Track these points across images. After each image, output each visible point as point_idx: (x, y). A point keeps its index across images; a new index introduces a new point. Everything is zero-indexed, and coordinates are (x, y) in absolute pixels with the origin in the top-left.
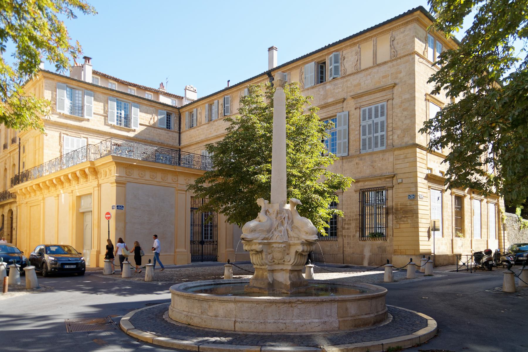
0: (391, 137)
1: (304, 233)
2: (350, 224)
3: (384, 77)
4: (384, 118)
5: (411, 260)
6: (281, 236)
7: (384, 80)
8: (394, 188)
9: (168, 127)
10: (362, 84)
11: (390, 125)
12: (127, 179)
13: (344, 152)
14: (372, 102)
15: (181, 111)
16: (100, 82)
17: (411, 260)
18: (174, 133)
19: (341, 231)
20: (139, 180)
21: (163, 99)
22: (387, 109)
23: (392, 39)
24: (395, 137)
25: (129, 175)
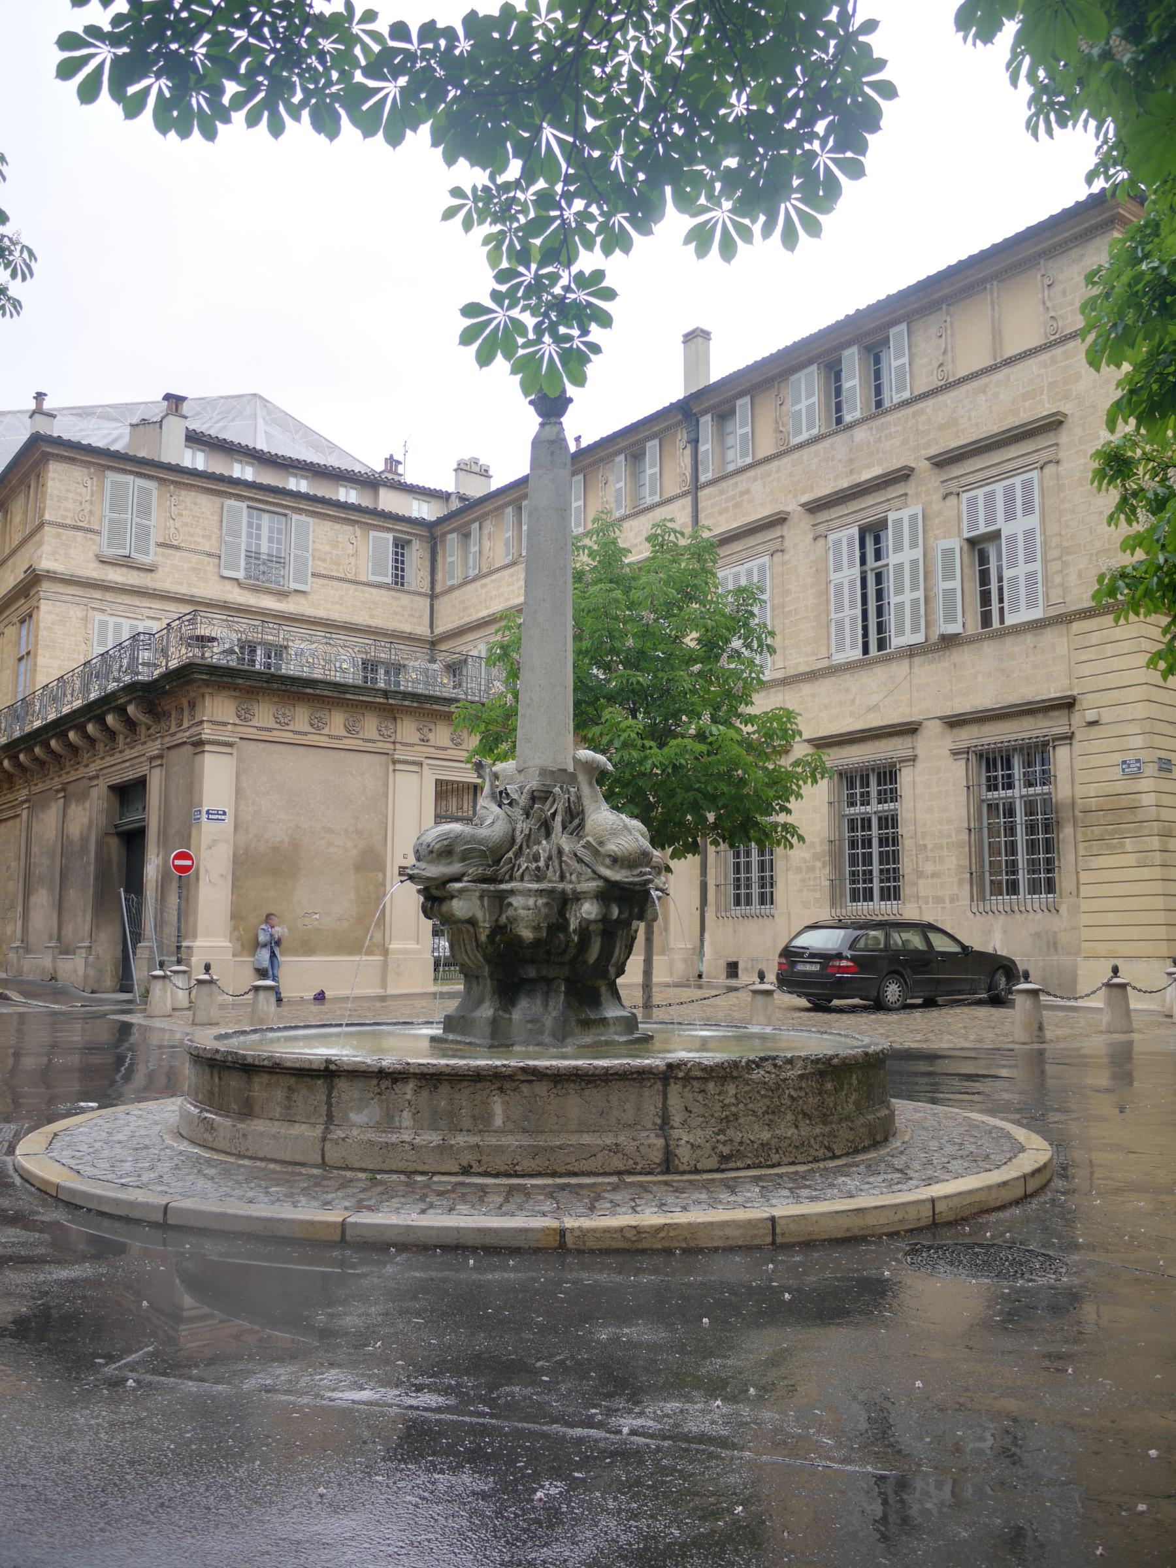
0: (1058, 579)
1: (607, 861)
2: (941, 858)
3: (1025, 396)
4: (1033, 521)
5: (1115, 970)
6: (538, 868)
7: (1027, 404)
8: (1075, 742)
9: (399, 579)
11: (1055, 541)
12: (240, 729)
13: (915, 629)
14: (994, 471)
15: (439, 531)
16: (198, 460)
17: (1115, 970)
18: (418, 598)
19: (915, 884)
20: (275, 733)
21: (388, 501)
22: (1042, 491)
24: (1073, 578)
25: (245, 720)
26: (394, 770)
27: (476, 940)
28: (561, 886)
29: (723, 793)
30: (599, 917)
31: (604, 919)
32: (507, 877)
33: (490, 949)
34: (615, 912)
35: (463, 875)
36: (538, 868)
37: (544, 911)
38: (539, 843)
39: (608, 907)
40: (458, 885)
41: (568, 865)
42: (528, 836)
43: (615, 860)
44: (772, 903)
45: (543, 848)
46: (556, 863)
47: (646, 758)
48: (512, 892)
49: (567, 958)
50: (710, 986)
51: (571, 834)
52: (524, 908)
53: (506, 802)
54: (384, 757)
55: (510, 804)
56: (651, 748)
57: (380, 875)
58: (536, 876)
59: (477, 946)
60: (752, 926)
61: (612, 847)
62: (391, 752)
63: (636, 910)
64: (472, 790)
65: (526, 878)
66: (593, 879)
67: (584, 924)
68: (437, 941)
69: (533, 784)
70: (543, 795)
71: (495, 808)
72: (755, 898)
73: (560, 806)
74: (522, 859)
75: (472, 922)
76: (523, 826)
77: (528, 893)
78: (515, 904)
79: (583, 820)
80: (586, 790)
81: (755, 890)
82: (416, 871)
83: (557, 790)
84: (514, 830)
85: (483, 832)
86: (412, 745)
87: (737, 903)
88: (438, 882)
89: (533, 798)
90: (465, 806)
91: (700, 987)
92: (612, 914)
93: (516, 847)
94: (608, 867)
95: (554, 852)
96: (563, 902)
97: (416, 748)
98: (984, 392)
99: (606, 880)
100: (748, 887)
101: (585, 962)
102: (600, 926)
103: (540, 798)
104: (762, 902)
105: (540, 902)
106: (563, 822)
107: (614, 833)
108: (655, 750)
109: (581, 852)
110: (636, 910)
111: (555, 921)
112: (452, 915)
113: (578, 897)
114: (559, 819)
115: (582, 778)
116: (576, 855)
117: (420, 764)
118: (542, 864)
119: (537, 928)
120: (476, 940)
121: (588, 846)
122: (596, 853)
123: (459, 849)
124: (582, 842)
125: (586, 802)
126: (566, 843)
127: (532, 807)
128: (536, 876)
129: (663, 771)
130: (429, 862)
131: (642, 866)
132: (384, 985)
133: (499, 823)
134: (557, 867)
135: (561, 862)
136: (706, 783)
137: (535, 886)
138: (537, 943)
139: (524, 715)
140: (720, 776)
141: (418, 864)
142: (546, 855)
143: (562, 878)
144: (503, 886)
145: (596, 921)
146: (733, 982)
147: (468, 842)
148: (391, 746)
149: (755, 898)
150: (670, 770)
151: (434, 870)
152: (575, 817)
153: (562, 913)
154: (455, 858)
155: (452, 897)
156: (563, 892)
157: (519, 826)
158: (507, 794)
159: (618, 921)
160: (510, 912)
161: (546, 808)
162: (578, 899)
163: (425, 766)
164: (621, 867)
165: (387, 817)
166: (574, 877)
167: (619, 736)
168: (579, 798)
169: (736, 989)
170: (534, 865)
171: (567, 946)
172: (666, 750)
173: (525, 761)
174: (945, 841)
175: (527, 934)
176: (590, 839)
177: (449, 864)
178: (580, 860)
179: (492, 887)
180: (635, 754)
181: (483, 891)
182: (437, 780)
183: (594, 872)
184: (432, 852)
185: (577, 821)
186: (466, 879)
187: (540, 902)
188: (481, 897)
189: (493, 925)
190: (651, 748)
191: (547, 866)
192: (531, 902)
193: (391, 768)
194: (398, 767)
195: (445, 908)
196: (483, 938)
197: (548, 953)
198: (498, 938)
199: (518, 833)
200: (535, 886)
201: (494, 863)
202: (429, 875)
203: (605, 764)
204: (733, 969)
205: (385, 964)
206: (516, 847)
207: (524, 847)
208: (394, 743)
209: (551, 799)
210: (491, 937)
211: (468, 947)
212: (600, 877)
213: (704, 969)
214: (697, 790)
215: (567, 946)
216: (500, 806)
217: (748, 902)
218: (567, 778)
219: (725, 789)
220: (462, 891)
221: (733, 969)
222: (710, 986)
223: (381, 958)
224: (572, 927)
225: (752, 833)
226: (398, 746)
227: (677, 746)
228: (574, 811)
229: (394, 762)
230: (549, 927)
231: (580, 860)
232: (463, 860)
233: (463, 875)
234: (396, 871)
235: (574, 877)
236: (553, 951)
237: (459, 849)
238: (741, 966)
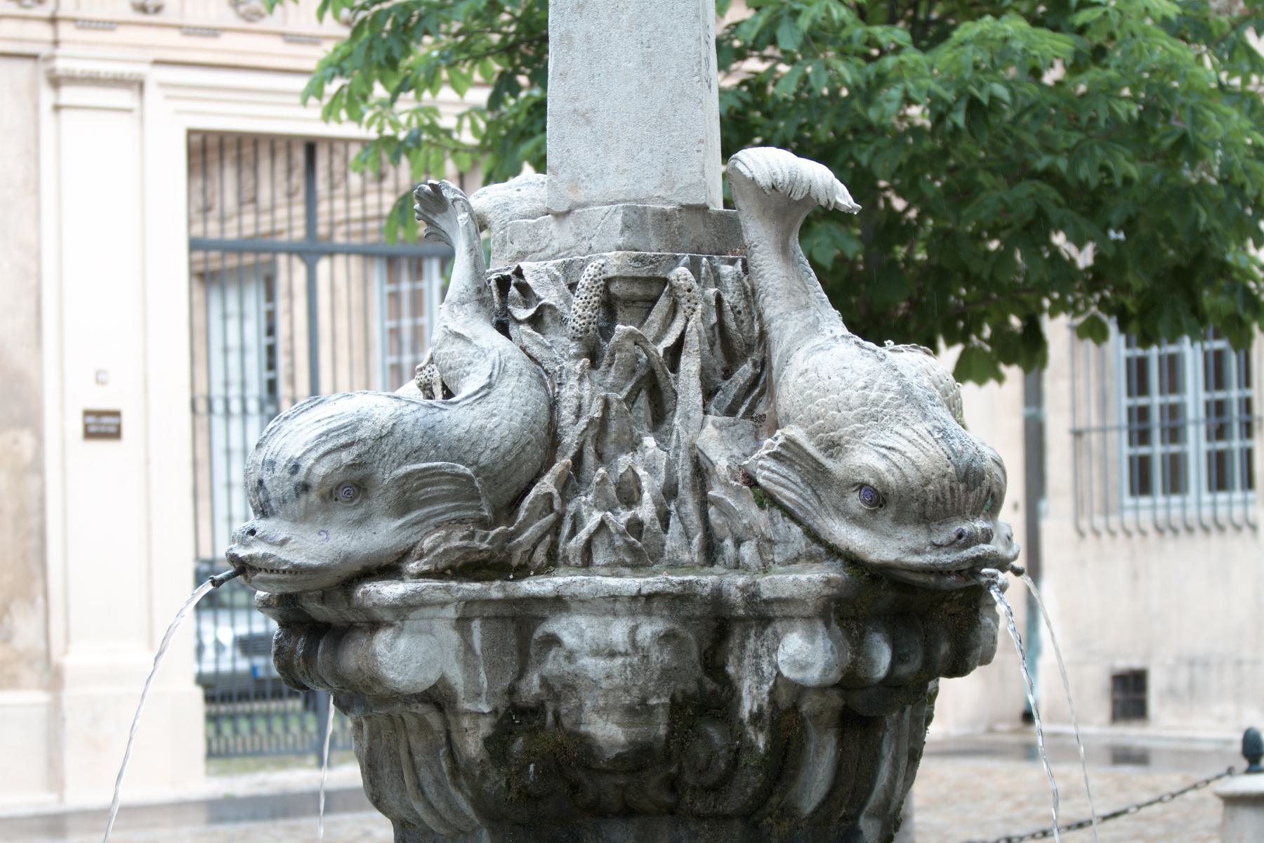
1: (854, 502)
26: (57, 108)
27: (452, 754)
28: (707, 580)
29: (1128, 181)
30: (835, 676)
31: (850, 682)
32: (540, 556)
33: (495, 781)
34: (882, 658)
35: (405, 555)
36: (636, 526)
37: (660, 657)
38: (634, 445)
39: (858, 643)
40: (390, 590)
41: (725, 511)
42: (601, 425)
43: (879, 500)
44: (1249, 483)
45: (649, 460)
46: (690, 507)
47: (882, 80)
48: (559, 603)
49: (734, 801)
50: (1063, 750)
51: (731, 411)
52: (596, 653)
53: (522, 313)
54: (25, 67)
55: (536, 322)
56: (898, 49)
57: (27, 439)
58: (631, 549)
59: (455, 770)
60: (1189, 560)
61: (865, 459)
62: (44, 50)
63: (944, 648)
64: (300, 156)
65: (600, 557)
66: (811, 558)
67: (784, 699)
68: (207, 625)
69: (609, 258)
70: (637, 290)
71: (489, 337)
72: (1197, 471)
73: (694, 324)
74: (584, 501)
75: (438, 698)
76: (582, 394)
77: (610, 604)
78: (569, 639)
79: (764, 364)
80: (771, 270)
81: (1196, 446)
82: (258, 550)
83: (680, 274)
84: (553, 405)
85: (460, 418)
86: (110, 25)
87: (1141, 483)
88: (327, 580)
89: (610, 304)
90: (265, 195)
91: (1029, 752)
92: (872, 664)
93: (562, 463)
94: (856, 520)
95: (683, 472)
96: (717, 629)
97: (123, 34)
99: (852, 561)
100: (1174, 434)
101: (788, 812)
102: (836, 700)
103: (630, 301)
104: (1219, 480)
105: (649, 630)
106: (705, 376)
107: (873, 416)
108: (912, 56)
109: (768, 474)
110: (944, 648)
111: (692, 687)
112: (376, 679)
113: (764, 615)
114: (690, 365)
115: (758, 233)
116: (751, 481)
117: (138, 85)
118: (646, 511)
119: (638, 711)
120: (452, 754)
121: (789, 454)
122: (817, 476)
123: (389, 473)
124: (770, 444)
125: (774, 308)
126: (717, 443)
127: (606, 332)
128: (631, 549)
129: (939, 119)
130: (296, 520)
131: (960, 513)
132: (55, 777)
133: (508, 386)
134: (694, 520)
135: (704, 503)
136: (1074, 153)
137: (630, 583)
138: (638, 758)
139: (567, 38)
140: (1117, 132)
141: (262, 525)
142: (659, 482)
143: (711, 552)
144: (531, 586)
145: (821, 689)
146: (1131, 734)
147: (415, 454)
148: (45, 32)
149: (1197, 471)
150: (959, 118)
151: (313, 545)
152: (741, 363)
153: (713, 664)
154: (378, 502)
155: (375, 625)
156: (718, 598)
157: (569, 394)
158: (524, 289)
159: (892, 683)
160: (553, 665)
161: (650, 332)
162: (764, 621)
163: (150, 88)
164: (899, 520)
165: (38, 256)
166: (748, 551)
167: (795, 14)
168: (750, 295)
169: (1139, 758)
170: (624, 516)
171: (734, 764)
172: (944, 54)
173: (574, 185)
175: (608, 732)
176: (796, 432)
177: (360, 522)
178: (766, 499)
179: (495, 590)
180: (846, 71)
181: (469, 602)
182: (190, 132)
183: (813, 535)
184: (305, 487)
185: (745, 371)
186: (413, 566)
187: (649, 630)
188: (462, 623)
189: (502, 704)
190: (898, 49)
191: (664, 517)
192: (618, 632)
193: (47, 97)
194: (69, 95)
195: (352, 658)
196: (472, 746)
197: (673, 785)
198: (518, 745)
199: (566, 414)
200: (630, 583)
201: (495, 514)
202: (299, 559)
203: (830, 190)
204: (1130, 693)
205: (55, 713)
206: (562, 463)
207: (590, 458)
208: (53, 20)
209: (663, 303)
210: (497, 744)
211: (426, 776)
212: (834, 552)
213: (1044, 695)
214: (1048, 175)
215: (734, 764)
216: (503, 328)
217: (1176, 483)
218: (714, 232)
219: (1134, 171)
220: (404, 608)
221: (1130, 693)
222: (1063, 750)
223: (41, 697)
224: (747, 706)
225: (1208, 298)
226: (66, 30)
227: (982, 39)
228: (738, 338)
229: (56, 82)
230: (676, 707)
231: (766, 499)
232: (403, 507)
233: (405, 555)
234: (76, 426)
235: (748, 551)
236: (689, 778)
237: (389, 473)
238: (1155, 684)
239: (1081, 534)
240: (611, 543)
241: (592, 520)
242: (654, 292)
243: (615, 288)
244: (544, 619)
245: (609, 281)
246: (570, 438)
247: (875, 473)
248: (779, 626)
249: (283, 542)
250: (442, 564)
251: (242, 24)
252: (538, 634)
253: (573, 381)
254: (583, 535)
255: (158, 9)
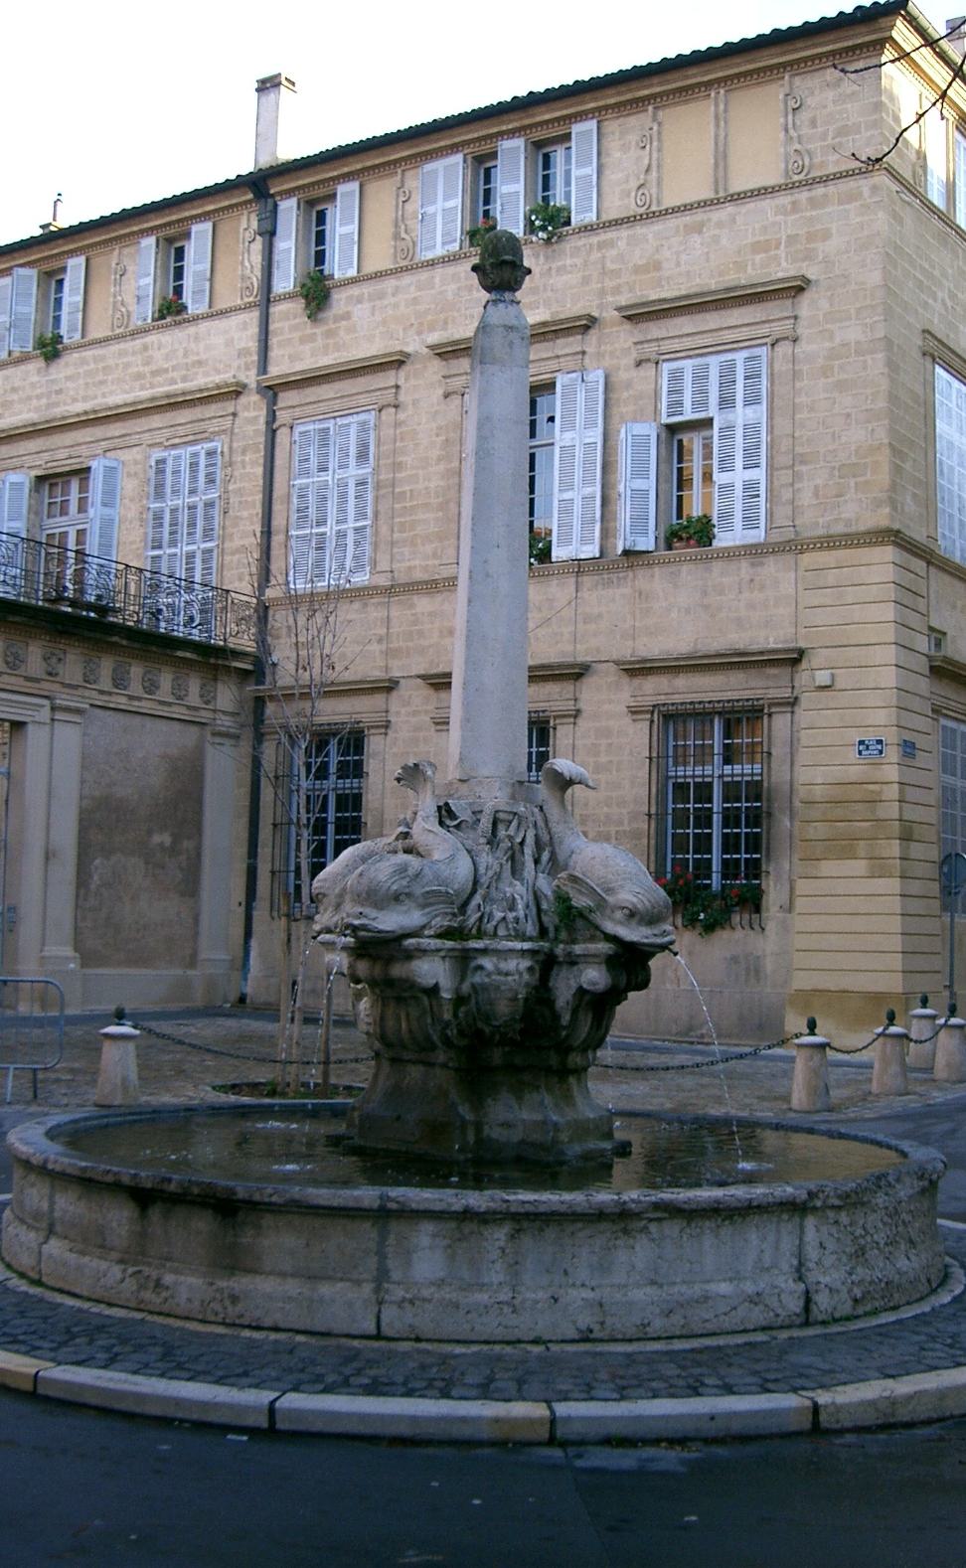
10: (665, 265)
23: (792, 104)
32: (474, 931)
75: (434, 991)
97: (80, 692)
98: (700, 232)
174: (613, 829)
187: (525, 963)
194: (58, 716)
199: (482, 870)
233: (424, 927)
239: (273, 918)
240: (507, 927)
241: (499, 915)
242: (511, 817)
243: (501, 816)
244: (475, 958)
245: (497, 812)
246: (484, 880)
247: (633, 903)
248: (581, 966)
249: (374, 919)
250: (439, 931)
251: (9, 671)
252: (473, 964)
253: (484, 854)
254: (494, 923)
255: (57, 674)
